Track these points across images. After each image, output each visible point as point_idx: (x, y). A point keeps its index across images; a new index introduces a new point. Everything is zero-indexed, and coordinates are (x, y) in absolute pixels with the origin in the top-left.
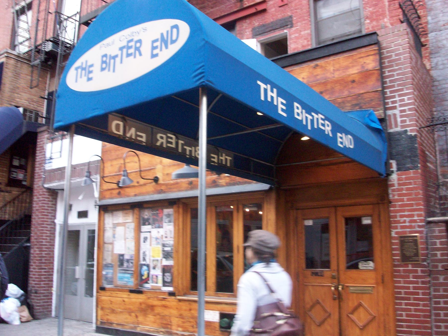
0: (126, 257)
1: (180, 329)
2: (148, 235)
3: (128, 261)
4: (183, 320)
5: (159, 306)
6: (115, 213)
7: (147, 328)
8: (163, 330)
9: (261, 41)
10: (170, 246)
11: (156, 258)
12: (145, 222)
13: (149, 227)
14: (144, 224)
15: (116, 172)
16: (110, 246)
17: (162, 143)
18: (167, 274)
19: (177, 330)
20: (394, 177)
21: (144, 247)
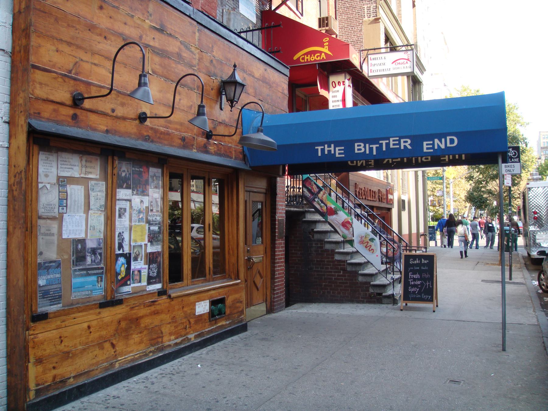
0: (90, 244)
1: (173, 337)
2: (127, 205)
3: (94, 251)
4: (175, 325)
5: (147, 316)
6: (65, 156)
7: (129, 357)
8: (152, 349)
10: (156, 224)
11: (139, 243)
12: (124, 183)
13: (129, 192)
14: (121, 187)
15: (70, 72)
16: (54, 226)
18: (154, 266)
19: (170, 340)
21: (122, 224)
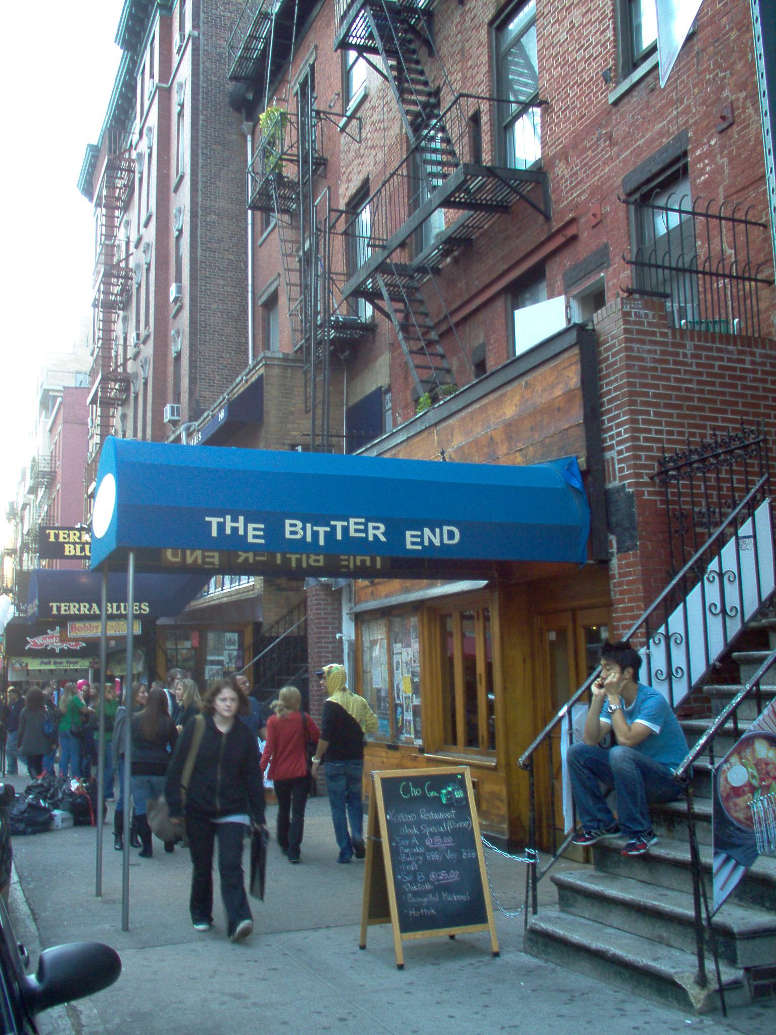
9: (579, 294)
17: (247, 559)
20: (614, 562)
